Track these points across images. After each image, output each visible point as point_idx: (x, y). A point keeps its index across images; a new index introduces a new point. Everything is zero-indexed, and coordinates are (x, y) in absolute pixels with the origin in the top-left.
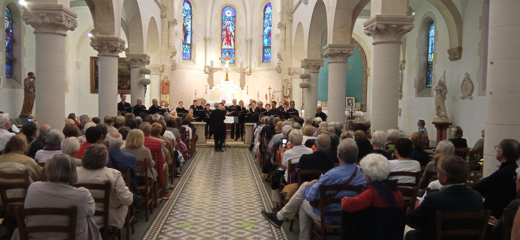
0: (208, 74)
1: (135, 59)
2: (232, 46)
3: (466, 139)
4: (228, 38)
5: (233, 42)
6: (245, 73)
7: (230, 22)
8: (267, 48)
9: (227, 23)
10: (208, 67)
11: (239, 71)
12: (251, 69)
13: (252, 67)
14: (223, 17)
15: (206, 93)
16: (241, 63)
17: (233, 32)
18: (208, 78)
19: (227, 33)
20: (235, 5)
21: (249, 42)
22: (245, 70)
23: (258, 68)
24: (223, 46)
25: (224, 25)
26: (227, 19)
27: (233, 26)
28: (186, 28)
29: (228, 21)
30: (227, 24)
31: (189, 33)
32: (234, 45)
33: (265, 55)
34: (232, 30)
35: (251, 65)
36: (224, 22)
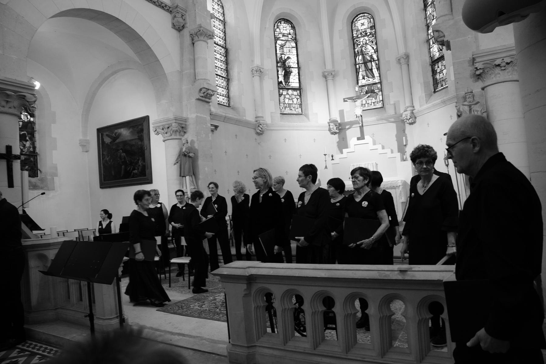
0: (337, 135)
1: (7, 92)
2: (376, 78)
3: (249, 195)
4: (366, 66)
5: (376, 70)
6: (403, 121)
7: (366, 38)
8: (438, 62)
9: (361, 40)
10: (335, 122)
11: (392, 120)
12: (414, 111)
13: (415, 107)
14: (354, 33)
15: (326, 167)
16: (394, 104)
17: (375, 52)
18: (338, 142)
19: (364, 58)
20: (369, 6)
21: (402, 61)
22: (401, 116)
23: (426, 106)
24: (360, 82)
25: (358, 45)
26: (361, 34)
27: (372, 43)
28: (286, 63)
29: (364, 36)
30: (361, 43)
31: (295, 71)
32: (378, 75)
33: (438, 77)
34: (373, 51)
35: (413, 104)
36: (357, 40)
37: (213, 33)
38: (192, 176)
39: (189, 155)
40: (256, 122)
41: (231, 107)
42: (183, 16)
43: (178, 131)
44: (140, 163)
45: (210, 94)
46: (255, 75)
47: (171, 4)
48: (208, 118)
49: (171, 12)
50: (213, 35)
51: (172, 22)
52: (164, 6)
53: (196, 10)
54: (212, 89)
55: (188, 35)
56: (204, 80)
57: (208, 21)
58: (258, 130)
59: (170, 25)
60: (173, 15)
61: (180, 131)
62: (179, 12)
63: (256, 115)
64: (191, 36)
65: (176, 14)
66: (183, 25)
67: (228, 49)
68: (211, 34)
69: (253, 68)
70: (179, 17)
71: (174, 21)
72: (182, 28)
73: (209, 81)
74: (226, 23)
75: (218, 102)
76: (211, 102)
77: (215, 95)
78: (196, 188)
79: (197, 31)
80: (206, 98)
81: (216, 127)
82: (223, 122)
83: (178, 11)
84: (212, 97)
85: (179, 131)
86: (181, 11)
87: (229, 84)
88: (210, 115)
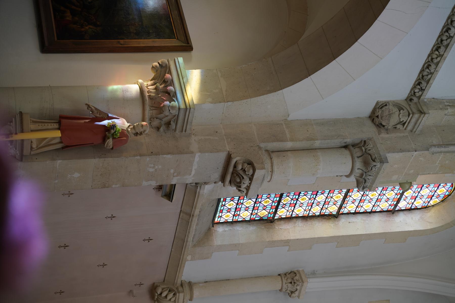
37: (371, 189)
38: (61, 142)
39: (109, 138)
40: (179, 282)
41: (213, 226)
42: (404, 124)
43: (161, 113)
44: (87, 28)
45: (240, 182)
46: (283, 278)
47: (425, 100)
48: (190, 179)
49: (409, 99)
50: (366, 187)
51: (388, 102)
52: (422, 85)
53: (416, 151)
54: (251, 187)
55: (364, 136)
56: (270, 170)
57: (395, 177)
58: (163, 289)
59: (383, 99)
60: (405, 104)
61: (161, 119)
62: (411, 115)
63: (195, 283)
64: (361, 141)
65: (405, 111)
66: (384, 126)
67: (337, 219)
68: (368, 184)
69: (298, 275)
70: (400, 117)
71: (391, 107)
72: (377, 123)
73: (269, 182)
74: (393, 213)
75: (222, 199)
76: (224, 186)
77: (239, 192)
78: (32, 153)
79: (372, 155)
80: (233, 173)
81: (169, 196)
82: (179, 211)
83: (413, 114)
84: (235, 188)
85: (161, 116)
86: (413, 120)
87: (262, 222)
88: (195, 182)
